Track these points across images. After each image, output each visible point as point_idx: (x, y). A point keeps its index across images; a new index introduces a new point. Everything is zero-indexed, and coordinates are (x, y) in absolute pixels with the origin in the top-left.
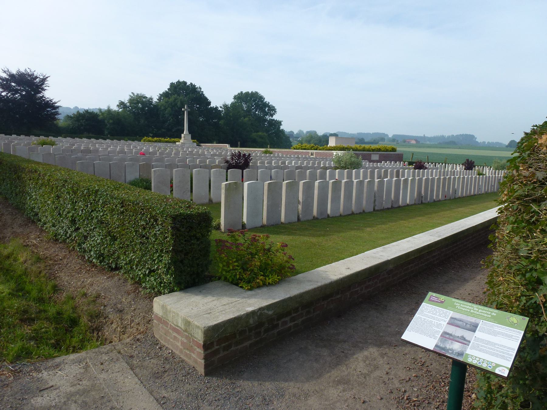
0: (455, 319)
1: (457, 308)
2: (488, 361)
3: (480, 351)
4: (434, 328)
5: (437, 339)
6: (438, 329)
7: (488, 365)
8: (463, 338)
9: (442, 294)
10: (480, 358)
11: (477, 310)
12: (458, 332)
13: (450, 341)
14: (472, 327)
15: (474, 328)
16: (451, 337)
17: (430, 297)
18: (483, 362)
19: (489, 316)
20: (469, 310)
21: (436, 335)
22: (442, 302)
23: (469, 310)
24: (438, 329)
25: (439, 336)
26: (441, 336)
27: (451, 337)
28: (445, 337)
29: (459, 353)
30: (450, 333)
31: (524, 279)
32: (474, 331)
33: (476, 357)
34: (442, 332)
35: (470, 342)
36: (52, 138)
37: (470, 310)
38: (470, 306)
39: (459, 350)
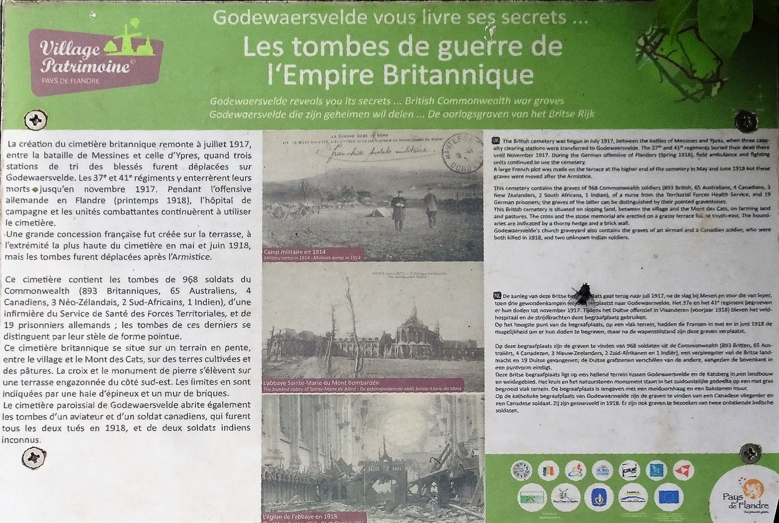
0: (302, 191)
1: (279, 88)
2: (642, 459)
3: (564, 398)
4: (188, 337)
5: (255, 423)
6: (221, 337)
7: (651, 487)
8: (421, 339)
9: (739, 45)
10: (589, 460)
11: (421, 48)
12: (372, 301)
13: (346, 404)
14: (442, 217)
15: (459, 219)
16: (344, 367)
17: (36, 59)
18: (616, 483)
19: (526, 77)
20: (366, 77)
21: (235, 394)
22: (145, 71)
23: (366, 77)
24: (221, 337)
25: (253, 393)
26: (270, 383)
27: (344, 367)
28: (304, 384)
29: (442, 479)
30: (320, 330)
31: (55, 53)
32: (473, 251)
33: (562, 460)
34: (255, 340)
35: (477, 354)
36: (718, 87)
37: (376, 64)
38: (359, 33)
39: (436, 446)
